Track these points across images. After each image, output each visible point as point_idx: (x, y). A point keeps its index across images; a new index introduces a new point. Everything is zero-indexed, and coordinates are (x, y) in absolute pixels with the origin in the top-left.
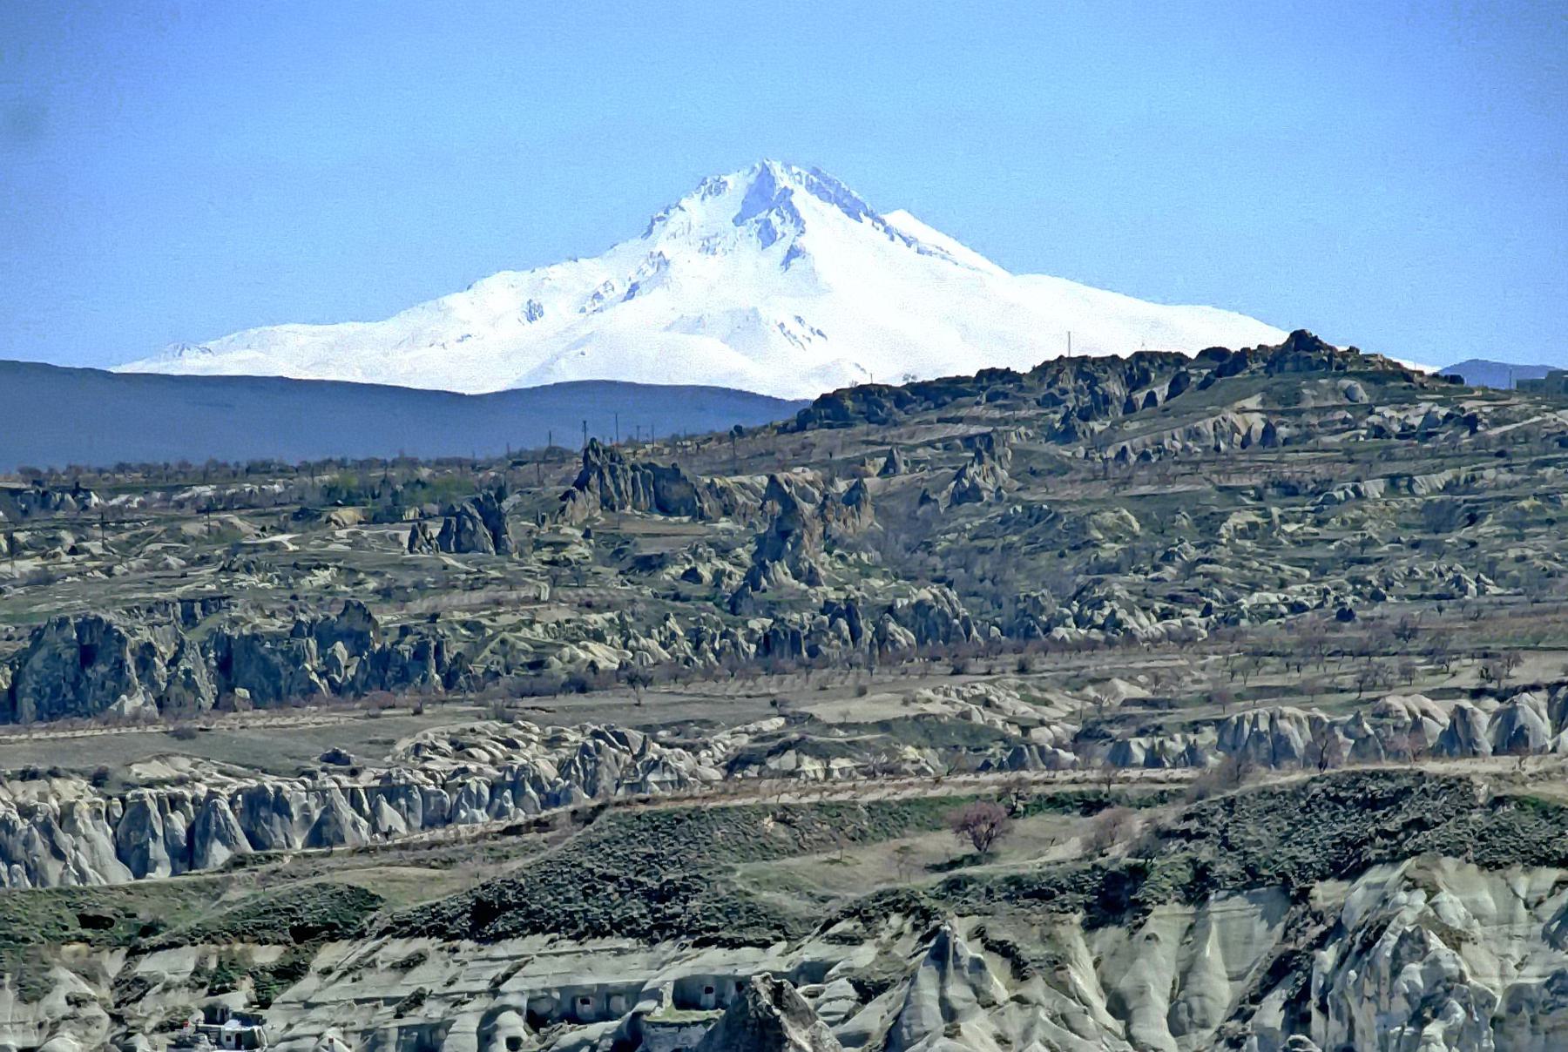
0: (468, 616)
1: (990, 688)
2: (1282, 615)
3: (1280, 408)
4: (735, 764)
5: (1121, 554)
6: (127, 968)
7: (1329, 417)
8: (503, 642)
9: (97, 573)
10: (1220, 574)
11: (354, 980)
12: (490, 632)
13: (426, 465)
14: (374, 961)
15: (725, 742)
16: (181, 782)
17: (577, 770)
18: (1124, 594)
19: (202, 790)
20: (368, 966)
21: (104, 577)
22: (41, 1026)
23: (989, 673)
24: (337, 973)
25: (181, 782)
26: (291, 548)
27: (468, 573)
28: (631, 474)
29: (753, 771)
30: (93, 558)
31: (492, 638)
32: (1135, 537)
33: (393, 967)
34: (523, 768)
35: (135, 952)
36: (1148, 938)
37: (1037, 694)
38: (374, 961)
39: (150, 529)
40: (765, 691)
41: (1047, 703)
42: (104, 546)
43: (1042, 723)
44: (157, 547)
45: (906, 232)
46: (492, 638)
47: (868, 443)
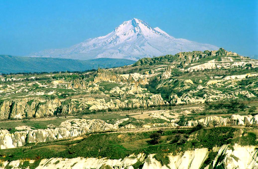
0: (76, 100)
1: (165, 112)
2: (217, 100)
3: (218, 62)
4: (120, 126)
5: (190, 87)
6: (9, 164)
7: (226, 64)
8: (82, 104)
9: (13, 92)
10: (207, 91)
11: (47, 166)
12: (80, 103)
13: (72, 72)
14: (50, 163)
15: (119, 122)
16: (24, 130)
17: (93, 128)
18: (190, 95)
19: (27, 132)
20: (49, 164)
21: (14, 93)
22: (173, 159)
23: (164, 110)
24: (44, 165)
25: (24, 130)
26: (47, 88)
27: (77, 92)
28: (105, 74)
29: (123, 127)
30: (13, 90)
31: (80, 104)
32: (192, 85)
33: (54, 163)
34: (83, 127)
35: (9, 161)
36: (184, 157)
37: (172, 113)
38: (50, 163)
39: (23, 84)
40: (125, 113)
41: (174, 115)
42: (15, 88)
43: (173, 119)
44: (24, 88)
45: (158, 31)
46: (80, 104)
47: (147, 68)
